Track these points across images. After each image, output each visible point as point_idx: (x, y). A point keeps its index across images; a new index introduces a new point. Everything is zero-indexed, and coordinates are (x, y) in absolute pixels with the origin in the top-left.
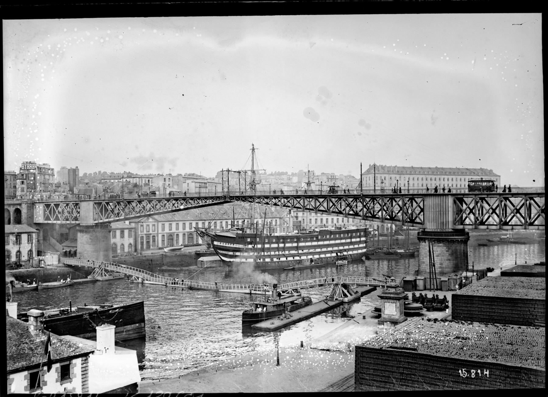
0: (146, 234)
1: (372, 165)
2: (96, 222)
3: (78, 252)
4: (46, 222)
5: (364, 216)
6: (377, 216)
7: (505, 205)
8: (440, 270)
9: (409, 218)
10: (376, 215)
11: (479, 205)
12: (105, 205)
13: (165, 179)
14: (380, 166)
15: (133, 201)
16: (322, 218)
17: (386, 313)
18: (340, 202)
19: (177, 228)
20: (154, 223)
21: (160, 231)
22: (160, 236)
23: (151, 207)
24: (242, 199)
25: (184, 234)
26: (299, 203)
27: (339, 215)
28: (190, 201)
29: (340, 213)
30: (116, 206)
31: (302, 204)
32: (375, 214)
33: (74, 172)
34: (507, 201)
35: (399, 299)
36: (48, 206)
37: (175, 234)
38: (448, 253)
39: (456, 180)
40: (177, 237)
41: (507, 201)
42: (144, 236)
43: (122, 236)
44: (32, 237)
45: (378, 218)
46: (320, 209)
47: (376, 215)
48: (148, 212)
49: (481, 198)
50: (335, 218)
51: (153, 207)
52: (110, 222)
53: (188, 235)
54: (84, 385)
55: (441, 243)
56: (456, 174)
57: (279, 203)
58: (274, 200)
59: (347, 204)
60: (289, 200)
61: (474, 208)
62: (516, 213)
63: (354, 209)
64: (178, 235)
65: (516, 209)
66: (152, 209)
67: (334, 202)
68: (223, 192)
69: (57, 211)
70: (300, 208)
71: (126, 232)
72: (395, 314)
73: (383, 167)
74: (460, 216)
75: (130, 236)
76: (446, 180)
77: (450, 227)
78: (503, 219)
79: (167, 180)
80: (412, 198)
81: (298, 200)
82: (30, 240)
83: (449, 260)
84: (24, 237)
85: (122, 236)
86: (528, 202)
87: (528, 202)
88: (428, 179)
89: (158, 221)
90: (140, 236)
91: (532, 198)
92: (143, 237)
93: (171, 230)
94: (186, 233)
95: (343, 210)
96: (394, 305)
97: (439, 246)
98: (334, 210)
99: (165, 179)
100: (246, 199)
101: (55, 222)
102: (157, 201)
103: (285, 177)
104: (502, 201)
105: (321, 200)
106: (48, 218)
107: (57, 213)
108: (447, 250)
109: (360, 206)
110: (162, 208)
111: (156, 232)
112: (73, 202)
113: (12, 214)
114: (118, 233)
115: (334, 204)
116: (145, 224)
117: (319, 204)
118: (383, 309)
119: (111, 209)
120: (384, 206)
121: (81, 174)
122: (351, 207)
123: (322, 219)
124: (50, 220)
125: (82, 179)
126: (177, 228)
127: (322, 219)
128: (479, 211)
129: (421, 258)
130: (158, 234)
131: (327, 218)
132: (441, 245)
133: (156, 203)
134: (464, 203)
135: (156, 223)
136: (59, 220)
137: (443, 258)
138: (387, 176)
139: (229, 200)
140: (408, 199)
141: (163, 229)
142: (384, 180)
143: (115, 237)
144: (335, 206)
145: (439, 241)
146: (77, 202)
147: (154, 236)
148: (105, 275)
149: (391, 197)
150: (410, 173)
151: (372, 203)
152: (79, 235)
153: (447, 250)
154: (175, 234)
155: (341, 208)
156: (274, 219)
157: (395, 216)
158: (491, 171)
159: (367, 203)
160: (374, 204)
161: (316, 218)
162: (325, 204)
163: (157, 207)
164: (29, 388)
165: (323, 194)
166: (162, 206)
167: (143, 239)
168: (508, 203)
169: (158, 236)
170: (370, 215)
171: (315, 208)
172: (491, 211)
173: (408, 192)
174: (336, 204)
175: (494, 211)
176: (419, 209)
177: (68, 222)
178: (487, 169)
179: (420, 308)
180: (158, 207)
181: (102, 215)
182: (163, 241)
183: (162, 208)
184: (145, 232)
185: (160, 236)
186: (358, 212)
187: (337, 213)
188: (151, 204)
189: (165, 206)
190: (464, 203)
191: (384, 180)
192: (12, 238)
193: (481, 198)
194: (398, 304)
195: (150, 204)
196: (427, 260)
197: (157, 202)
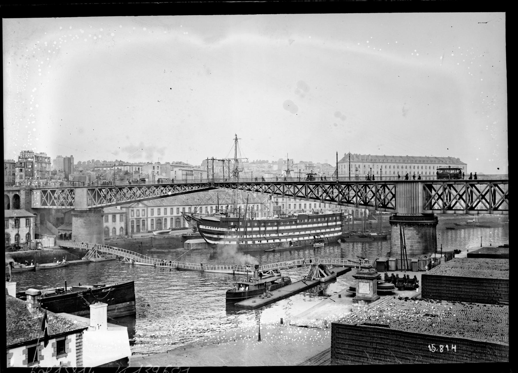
0: (136, 219)
1: (347, 154)
2: (90, 207)
3: (72, 235)
4: (43, 207)
5: (340, 201)
6: (352, 202)
7: (471, 192)
8: (411, 252)
9: (382, 204)
10: (351, 200)
11: (447, 191)
12: (98, 191)
13: (154, 167)
14: (354, 154)
15: (124, 188)
16: (300, 203)
17: (360, 292)
18: (317, 188)
19: (165, 213)
20: (143, 208)
21: (149, 216)
22: (149, 220)
23: (141, 194)
24: (226, 186)
25: (172, 219)
26: (279, 189)
27: (316, 200)
28: (178, 187)
29: (317, 198)
30: (108, 192)
31: (282, 190)
32: (350, 199)
33: (69, 160)
34: (473, 187)
35: (372, 279)
36: (45, 192)
37: (164, 218)
38: (418, 236)
39: (426, 168)
40: (165, 222)
41: (473, 187)
42: (135, 220)
43: (114, 220)
44: (29, 221)
45: (353, 203)
46: (298, 195)
47: (351, 200)
48: (138, 198)
49: (449, 185)
50: (313, 203)
51: (143, 193)
52: (102, 207)
53: (176, 219)
54: (78, 359)
55: (411, 227)
56: (425, 162)
57: (261, 190)
58: (248, 186)
59: (324, 190)
60: (269, 186)
61: (442, 194)
62: (482, 199)
63: (331, 195)
64: (166, 219)
65: (482, 195)
66: (142, 195)
67: (312, 189)
68: (208, 179)
69: (53, 197)
70: (280, 194)
71: (118, 217)
72: (368, 292)
73: (357, 156)
74: (429, 201)
75: (121, 220)
76: (416, 168)
77: (420, 212)
78: (469, 205)
79: (156, 167)
80: (385, 184)
81: (278, 186)
82: (28, 224)
83: (419, 242)
84: (23, 221)
85: (114, 220)
86: (493, 189)
87: (493, 189)
88: (399, 167)
89: (147, 207)
90: (131, 220)
91: (496, 185)
92: (133, 221)
93: (160, 215)
94: (174, 218)
95: (320, 196)
96: (368, 284)
97: (409, 230)
98: (312, 196)
99: (154, 167)
100: (229, 186)
101: (51, 207)
102: (146, 187)
103: (266, 165)
104: (468, 188)
105: (300, 187)
106: (44, 204)
107: (53, 199)
108: (417, 233)
109: (336, 192)
110: (151, 194)
111: (146, 217)
112: (68, 189)
113: (11, 199)
114: (110, 217)
115: (311, 191)
116: (135, 209)
117: (298, 190)
118: (358, 288)
119: (104, 195)
120: (358, 192)
121: (75, 162)
122: (327, 193)
123: (300, 205)
124: (47, 205)
125: (77, 167)
126: (165, 213)
127: (300, 205)
128: (447, 197)
129: (393, 241)
130: (147, 218)
131: (305, 203)
132: (411, 228)
133: (145, 190)
134: (433, 189)
135: (145, 208)
136: (55, 205)
137: (413, 241)
138: (361, 164)
139: (214, 187)
140: (380, 186)
141: (152, 214)
142: (358, 167)
143: (107, 221)
144: (313, 192)
145: (410, 225)
146: (72, 189)
147: (144, 220)
148: (98, 257)
149: (365, 184)
150: (391, 162)
151: (347, 189)
152: (74, 219)
153: (417, 233)
154: (164, 218)
155: (318, 194)
156: (256, 205)
157: (369, 201)
158: (458, 159)
159: (343, 190)
160: (349, 190)
161: (295, 203)
162: (303, 191)
163: (146, 193)
164: (27, 362)
165: (302, 181)
166: (151, 192)
167: (133, 223)
168: (474, 189)
169: (147, 220)
170: (345, 201)
171: (294, 194)
172: (458, 197)
173: (381, 179)
174: (313, 190)
175: (461, 197)
176: (391, 195)
177: (63, 207)
178: (454, 158)
179: (392, 288)
180: (147, 193)
181: (95, 200)
182: (152, 225)
183: (151, 194)
184: (135, 217)
185: (149, 220)
186: (334, 197)
187: (314, 198)
188: (141, 190)
189: (154, 192)
190: (433, 189)
191: (358, 167)
192: (11, 222)
193: (449, 185)
194: (371, 284)
195: (140, 190)
196: (398, 242)
197: (147, 188)
